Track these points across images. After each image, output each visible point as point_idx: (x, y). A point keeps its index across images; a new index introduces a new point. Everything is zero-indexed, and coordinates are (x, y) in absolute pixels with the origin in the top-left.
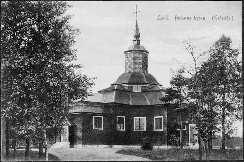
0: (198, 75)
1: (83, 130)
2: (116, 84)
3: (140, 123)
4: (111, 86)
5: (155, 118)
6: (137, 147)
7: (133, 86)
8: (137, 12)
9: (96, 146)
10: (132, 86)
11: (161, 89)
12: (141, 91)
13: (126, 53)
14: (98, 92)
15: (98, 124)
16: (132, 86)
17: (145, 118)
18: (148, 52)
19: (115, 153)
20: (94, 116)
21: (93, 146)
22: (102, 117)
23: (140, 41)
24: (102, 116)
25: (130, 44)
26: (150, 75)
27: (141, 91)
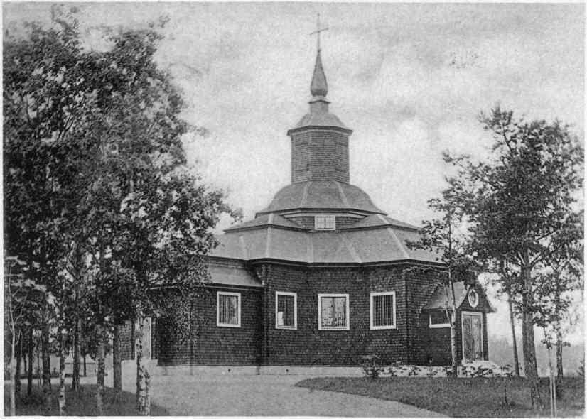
0: (550, 206)
1: (156, 325)
2: (269, 213)
3: (332, 309)
4: (256, 217)
5: (374, 297)
6: (358, 372)
7: (313, 217)
8: (319, 32)
9: (227, 368)
10: (312, 215)
11: (387, 222)
12: (334, 229)
13: (293, 134)
14: (225, 231)
15: (384, 318)
16: (312, 215)
17: (347, 296)
18: (350, 132)
19: (296, 385)
20: (219, 293)
21: (216, 369)
22: (295, 295)
23: (327, 103)
24: (238, 291)
25: (297, 109)
26: (355, 187)
27: (334, 229)
